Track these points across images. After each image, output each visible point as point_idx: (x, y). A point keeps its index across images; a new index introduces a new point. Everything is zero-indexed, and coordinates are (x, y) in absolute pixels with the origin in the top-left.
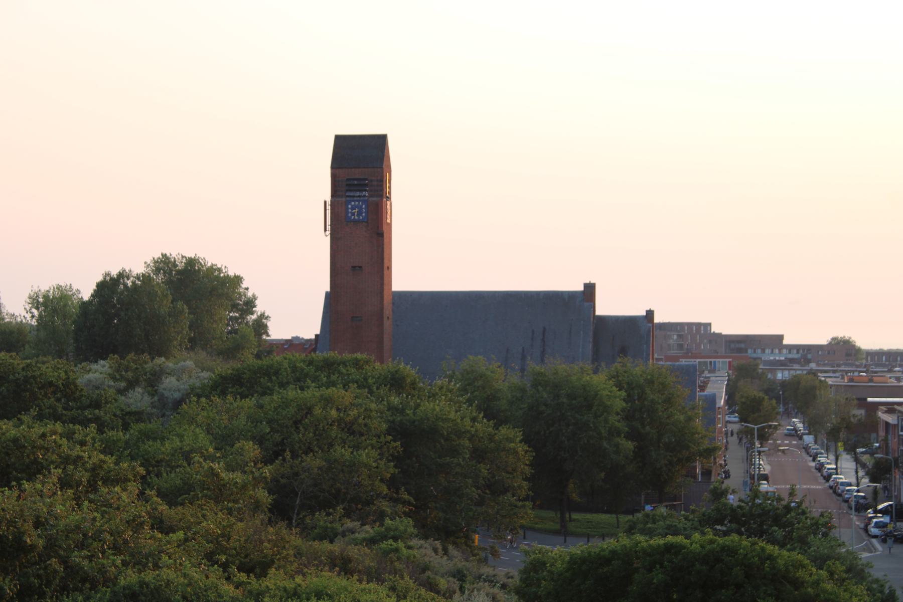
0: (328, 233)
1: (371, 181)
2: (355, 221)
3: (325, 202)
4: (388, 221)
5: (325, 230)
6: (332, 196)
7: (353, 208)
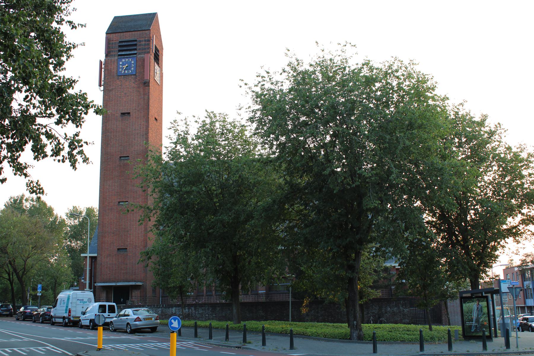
0: (102, 88)
1: (140, 41)
2: (125, 75)
3: (101, 62)
4: (157, 78)
5: (100, 85)
6: (107, 55)
7: (123, 65)
